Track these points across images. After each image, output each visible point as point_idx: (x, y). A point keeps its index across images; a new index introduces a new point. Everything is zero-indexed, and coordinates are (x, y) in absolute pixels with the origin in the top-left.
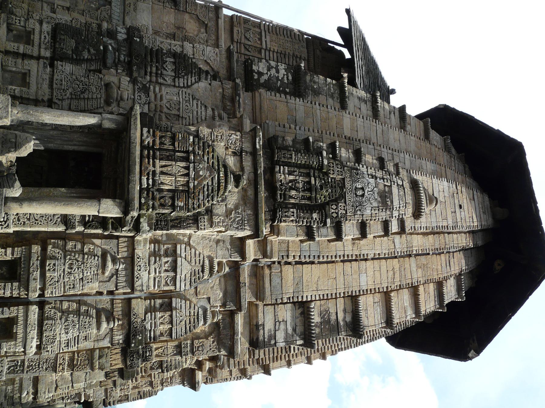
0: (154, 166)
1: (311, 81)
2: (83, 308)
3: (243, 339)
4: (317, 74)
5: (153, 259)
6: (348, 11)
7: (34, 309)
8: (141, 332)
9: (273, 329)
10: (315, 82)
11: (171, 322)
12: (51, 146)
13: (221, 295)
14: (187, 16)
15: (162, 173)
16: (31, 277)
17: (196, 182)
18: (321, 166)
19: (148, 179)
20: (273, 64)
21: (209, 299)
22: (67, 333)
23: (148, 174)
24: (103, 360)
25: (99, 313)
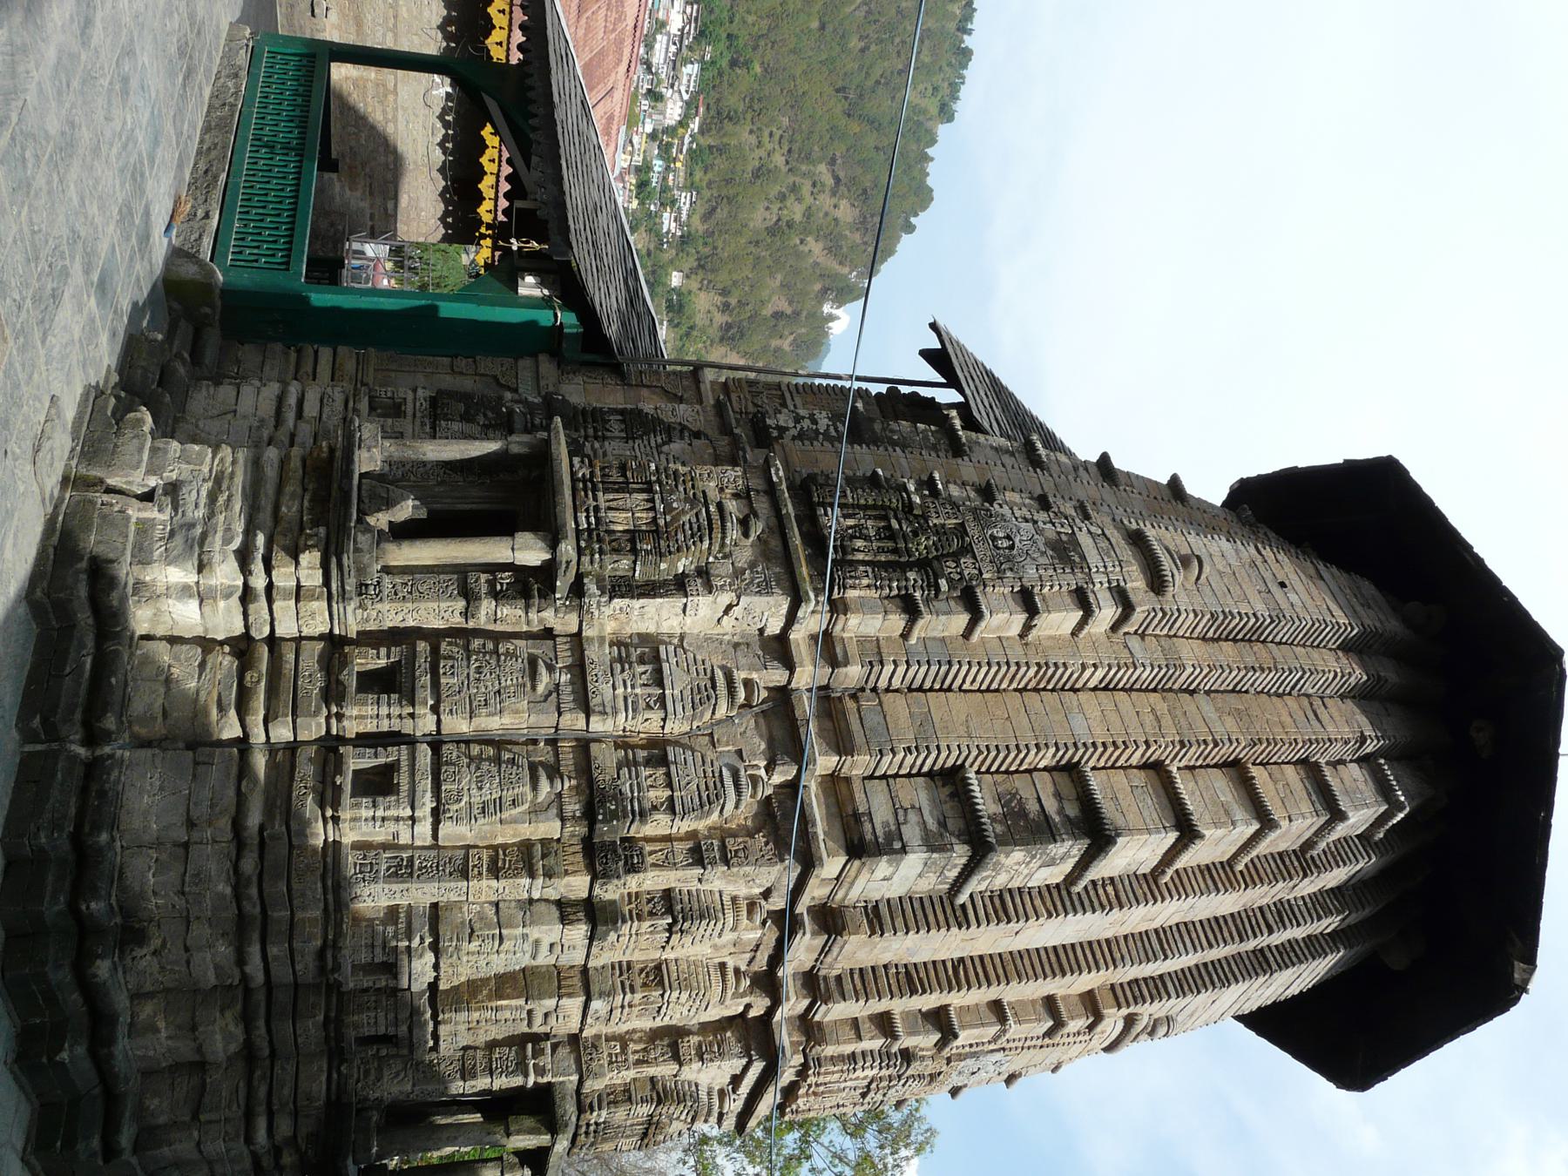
0: (595, 499)
1: (884, 429)
2: (506, 756)
3: (830, 844)
4: (896, 419)
5: (618, 667)
6: (934, 326)
7: (425, 754)
8: (614, 797)
9: (892, 821)
10: (892, 431)
11: (670, 785)
12: (437, 506)
13: (763, 746)
14: (645, 392)
15: (610, 508)
16: (418, 685)
17: (668, 518)
18: (909, 506)
19: (587, 517)
20: (802, 412)
21: (739, 753)
22: (480, 788)
23: (587, 510)
24: (551, 861)
25: (533, 768)
